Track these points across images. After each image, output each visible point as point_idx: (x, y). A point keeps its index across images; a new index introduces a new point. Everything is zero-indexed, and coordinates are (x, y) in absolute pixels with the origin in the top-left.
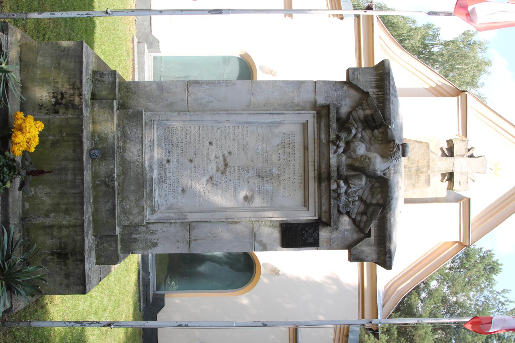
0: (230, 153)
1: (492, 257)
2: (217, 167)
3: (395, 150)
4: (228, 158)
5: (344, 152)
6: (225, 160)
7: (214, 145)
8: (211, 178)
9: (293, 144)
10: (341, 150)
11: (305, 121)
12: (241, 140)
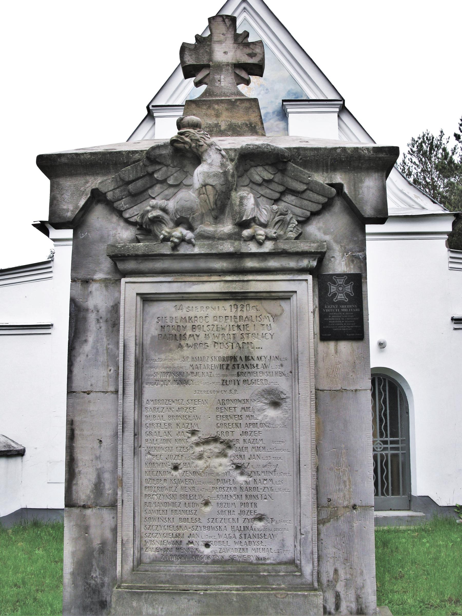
0: (193, 433)
1: (112, 471)
2: (217, 457)
3: (187, 139)
4: (203, 434)
5: (191, 228)
6: (207, 442)
7: (179, 462)
8: (238, 467)
9: (178, 321)
10: (189, 235)
11: (139, 298)
12: (171, 413)
